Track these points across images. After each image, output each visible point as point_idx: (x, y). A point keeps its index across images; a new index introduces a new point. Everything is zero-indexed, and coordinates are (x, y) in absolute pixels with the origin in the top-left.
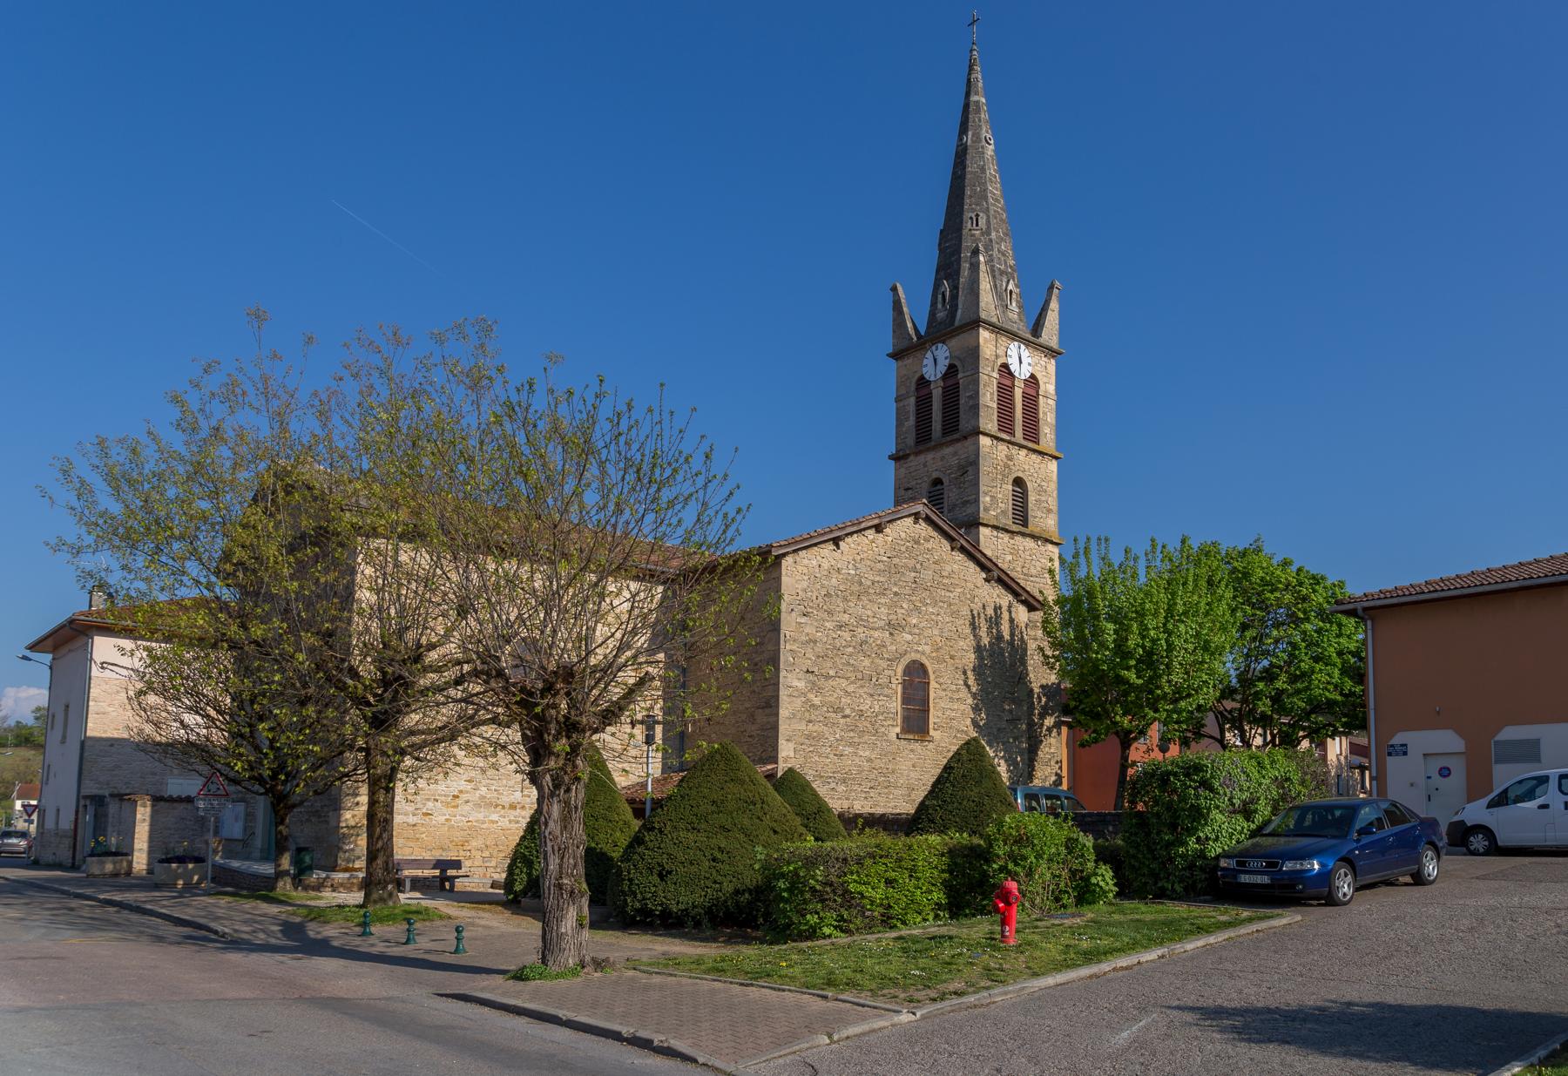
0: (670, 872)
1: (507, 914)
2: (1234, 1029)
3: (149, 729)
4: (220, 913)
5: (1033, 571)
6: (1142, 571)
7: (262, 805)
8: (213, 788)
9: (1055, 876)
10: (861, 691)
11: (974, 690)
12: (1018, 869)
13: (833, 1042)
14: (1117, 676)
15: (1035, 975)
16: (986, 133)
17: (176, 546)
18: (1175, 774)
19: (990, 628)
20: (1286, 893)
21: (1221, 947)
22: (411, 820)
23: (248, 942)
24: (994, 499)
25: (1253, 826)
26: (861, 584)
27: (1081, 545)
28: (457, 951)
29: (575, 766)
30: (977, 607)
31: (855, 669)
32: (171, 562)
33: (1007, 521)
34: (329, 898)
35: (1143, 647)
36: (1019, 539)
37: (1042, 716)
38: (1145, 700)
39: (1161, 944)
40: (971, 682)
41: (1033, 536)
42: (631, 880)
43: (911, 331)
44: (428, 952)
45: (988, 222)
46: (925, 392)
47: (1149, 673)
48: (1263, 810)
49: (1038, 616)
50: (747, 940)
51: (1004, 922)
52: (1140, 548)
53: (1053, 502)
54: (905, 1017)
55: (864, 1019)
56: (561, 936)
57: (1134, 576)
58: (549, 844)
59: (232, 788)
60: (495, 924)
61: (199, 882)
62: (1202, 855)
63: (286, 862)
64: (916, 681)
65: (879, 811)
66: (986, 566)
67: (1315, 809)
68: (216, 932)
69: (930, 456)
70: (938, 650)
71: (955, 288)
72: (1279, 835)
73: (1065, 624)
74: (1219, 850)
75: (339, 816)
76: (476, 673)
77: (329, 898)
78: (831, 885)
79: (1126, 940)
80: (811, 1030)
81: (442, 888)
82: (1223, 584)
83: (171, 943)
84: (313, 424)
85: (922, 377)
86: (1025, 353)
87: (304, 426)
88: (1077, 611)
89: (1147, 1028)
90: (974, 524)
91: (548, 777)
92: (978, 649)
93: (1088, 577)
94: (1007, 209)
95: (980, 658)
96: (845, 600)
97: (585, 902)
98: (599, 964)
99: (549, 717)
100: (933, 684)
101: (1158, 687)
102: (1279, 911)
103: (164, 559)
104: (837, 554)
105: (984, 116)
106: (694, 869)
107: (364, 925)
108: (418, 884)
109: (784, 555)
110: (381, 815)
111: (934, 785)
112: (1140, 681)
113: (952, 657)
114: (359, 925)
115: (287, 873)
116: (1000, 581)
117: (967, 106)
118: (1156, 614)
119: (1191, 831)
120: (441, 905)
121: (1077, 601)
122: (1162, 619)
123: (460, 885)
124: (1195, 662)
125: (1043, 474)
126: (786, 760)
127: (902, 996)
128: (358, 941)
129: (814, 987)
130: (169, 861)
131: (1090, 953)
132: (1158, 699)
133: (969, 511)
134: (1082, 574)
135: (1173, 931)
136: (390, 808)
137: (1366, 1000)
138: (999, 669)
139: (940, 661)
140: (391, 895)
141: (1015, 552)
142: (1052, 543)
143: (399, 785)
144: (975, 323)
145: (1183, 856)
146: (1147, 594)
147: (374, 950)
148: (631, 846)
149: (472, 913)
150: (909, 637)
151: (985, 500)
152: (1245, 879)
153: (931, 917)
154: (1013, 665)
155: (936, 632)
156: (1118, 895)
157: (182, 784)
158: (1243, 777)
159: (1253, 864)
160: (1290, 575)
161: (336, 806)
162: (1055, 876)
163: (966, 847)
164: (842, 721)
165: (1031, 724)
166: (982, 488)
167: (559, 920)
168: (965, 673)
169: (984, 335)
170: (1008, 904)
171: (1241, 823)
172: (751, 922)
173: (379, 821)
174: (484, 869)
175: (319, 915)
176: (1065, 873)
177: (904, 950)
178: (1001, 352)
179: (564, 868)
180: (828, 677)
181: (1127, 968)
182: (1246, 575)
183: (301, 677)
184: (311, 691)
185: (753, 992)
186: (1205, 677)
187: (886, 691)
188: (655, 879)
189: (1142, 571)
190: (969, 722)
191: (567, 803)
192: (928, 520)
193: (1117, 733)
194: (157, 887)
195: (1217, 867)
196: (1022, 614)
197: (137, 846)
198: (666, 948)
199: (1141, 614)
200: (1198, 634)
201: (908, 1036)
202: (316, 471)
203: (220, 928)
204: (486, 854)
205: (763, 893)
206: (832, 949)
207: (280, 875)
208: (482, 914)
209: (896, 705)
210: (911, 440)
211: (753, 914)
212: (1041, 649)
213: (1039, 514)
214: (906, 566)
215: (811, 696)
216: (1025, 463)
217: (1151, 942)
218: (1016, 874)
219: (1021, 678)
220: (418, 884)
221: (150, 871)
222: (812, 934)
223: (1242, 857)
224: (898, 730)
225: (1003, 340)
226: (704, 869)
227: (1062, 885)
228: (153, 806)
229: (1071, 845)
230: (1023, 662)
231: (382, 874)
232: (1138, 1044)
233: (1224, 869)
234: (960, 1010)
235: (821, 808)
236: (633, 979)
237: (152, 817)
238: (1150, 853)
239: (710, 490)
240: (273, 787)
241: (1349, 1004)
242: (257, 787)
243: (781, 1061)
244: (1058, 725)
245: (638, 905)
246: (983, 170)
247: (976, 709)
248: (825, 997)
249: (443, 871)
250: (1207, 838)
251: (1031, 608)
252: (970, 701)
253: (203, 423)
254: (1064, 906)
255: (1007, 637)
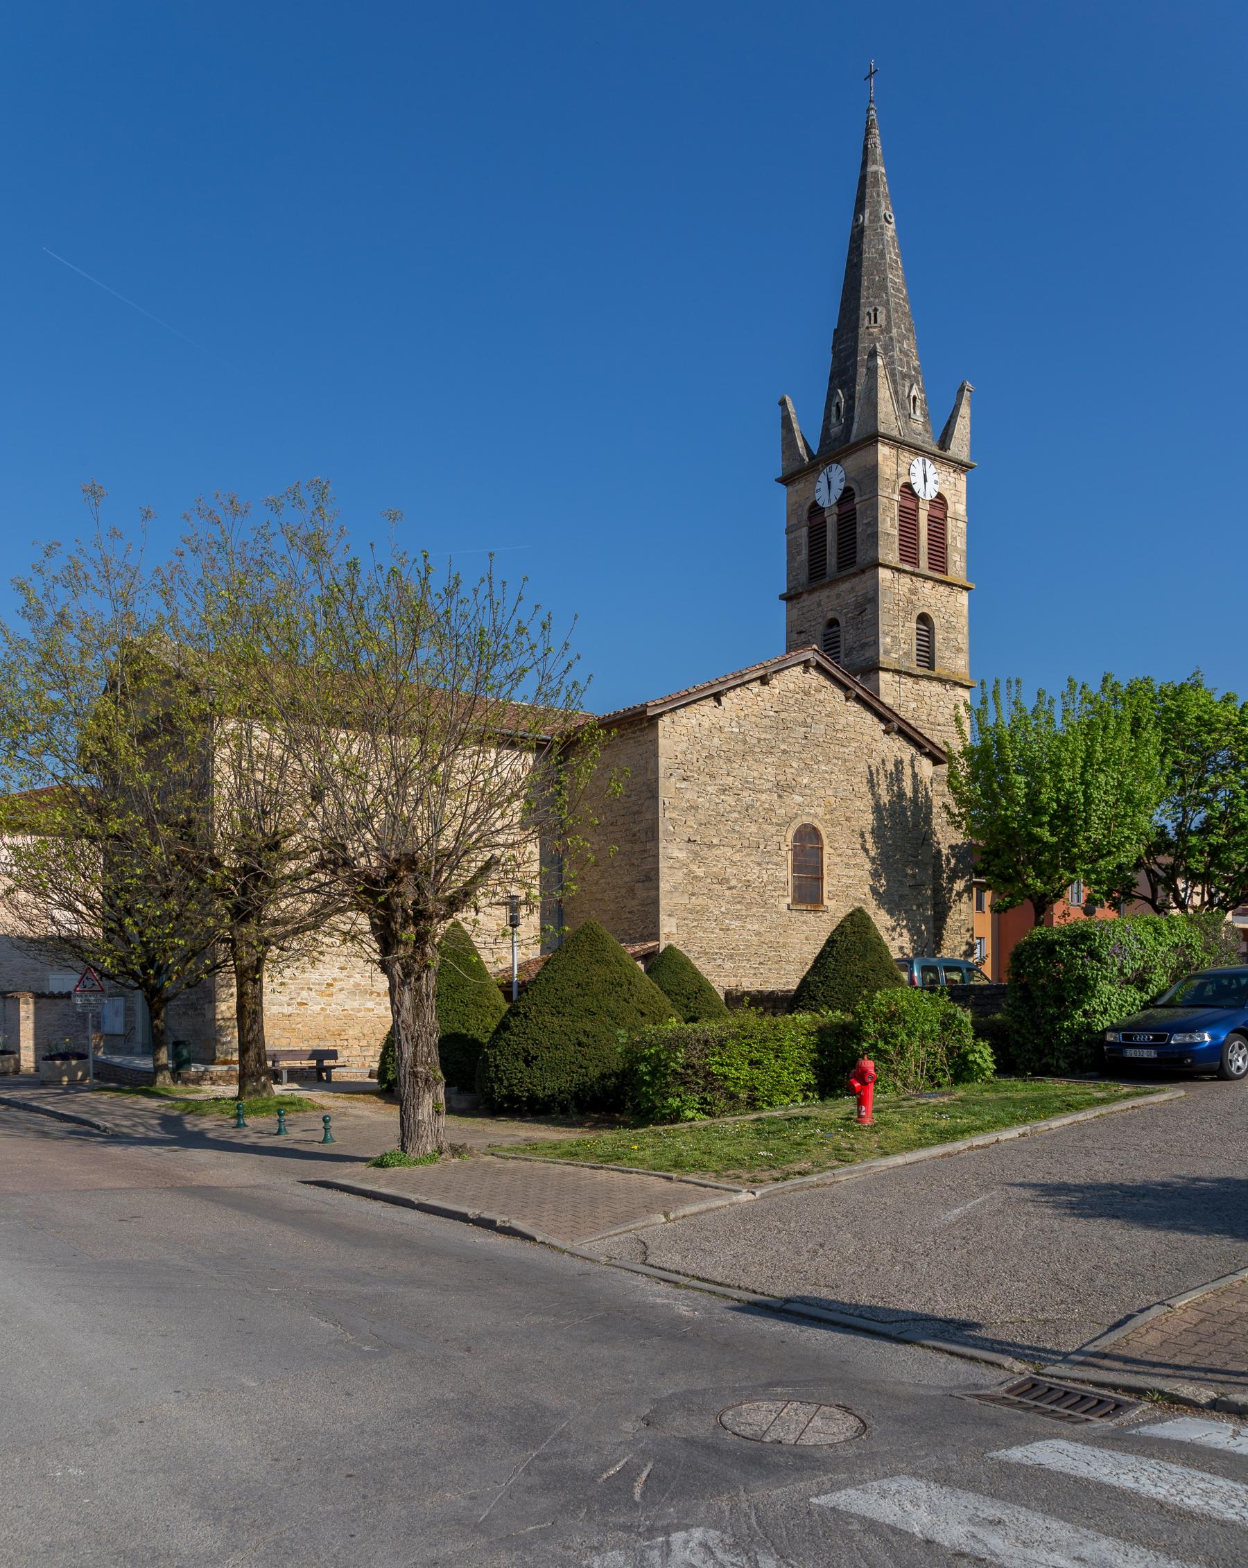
0: (535, 1058)
1: (381, 1103)
2: (1071, 1206)
3: (23, 928)
4: (102, 1108)
5: (941, 719)
6: (1057, 714)
7: (139, 996)
8: (88, 984)
9: (929, 1054)
10: (748, 860)
11: (873, 854)
12: (889, 1048)
13: (669, 1221)
14: (1030, 834)
15: (886, 1154)
16: (885, 209)
17: (31, 739)
18: (1061, 944)
19: (890, 785)
20: (1176, 1067)
21: (1090, 1124)
22: (286, 1010)
23: (128, 1136)
24: (895, 640)
25: (1146, 997)
26: (745, 742)
27: (989, 689)
28: (325, 1141)
29: (424, 954)
30: (875, 762)
31: (741, 836)
32: (27, 757)
33: (911, 665)
34: (208, 1090)
35: (1058, 801)
36: (924, 684)
37: (952, 880)
38: (1062, 859)
39: (1024, 1122)
40: (869, 845)
41: (940, 680)
42: (497, 1066)
43: (802, 451)
44: (298, 1142)
45: (888, 317)
46: (818, 520)
47: (1065, 830)
48: (1160, 979)
49: (943, 769)
50: (612, 1124)
51: (861, 1102)
52: (1055, 689)
53: (963, 640)
54: (744, 1197)
55: (703, 1198)
56: (418, 1124)
57: (1050, 721)
58: (403, 1033)
59: (106, 983)
60: (367, 1113)
61: (83, 1078)
62: (1088, 1029)
63: (164, 1056)
64: (808, 846)
65: (769, 987)
66: (885, 716)
67: (1215, 977)
68: (98, 1127)
69: (824, 594)
70: (831, 812)
71: (850, 398)
72: (1173, 1007)
73: (973, 778)
74: (1107, 1024)
75: (215, 1008)
76: (322, 865)
77: (208, 1090)
78: (693, 1067)
79: (988, 1118)
80: (649, 1209)
81: (320, 1079)
82: (1150, 726)
83: (55, 1139)
84: (157, 602)
85: (815, 504)
86: (931, 469)
87: (149, 607)
88: (987, 761)
89: (982, 1205)
90: (872, 669)
91: (398, 966)
92: (877, 809)
93: (996, 725)
94: (910, 299)
95: (879, 819)
96: (729, 760)
97: (441, 1089)
98: (456, 1150)
99: (400, 906)
100: (827, 850)
101: (1075, 845)
102: (1158, 1087)
103: (20, 753)
104: (719, 711)
105: (883, 189)
106: (559, 1054)
107: (238, 1116)
108: (295, 1075)
109: (661, 715)
110: (250, 1006)
111: (817, 960)
112: (1055, 839)
113: (848, 819)
114: (234, 1117)
115: (165, 1067)
116: (901, 732)
117: (863, 178)
118: (1072, 765)
119: (1077, 1004)
120: (318, 1096)
121: (984, 752)
122: (1078, 770)
123: (337, 1075)
124: (1116, 816)
125: (952, 608)
126: (668, 937)
127: (746, 1176)
128: (232, 1133)
129: (660, 1169)
130: (52, 1058)
131: (947, 1132)
132: (1074, 859)
133: (867, 655)
134: (990, 722)
135: (1042, 1108)
136: (258, 998)
137: (1216, 1175)
138: (900, 835)
139: (834, 823)
140: (264, 1086)
141: (919, 698)
142: (962, 686)
143: (266, 975)
144: (873, 438)
145: (1068, 1030)
146: (1063, 741)
147: (246, 1141)
148: (497, 1032)
149: (346, 1103)
150: (799, 799)
151: (885, 641)
152: (1131, 1053)
153: (799, 1099)
154: (916, 825)
155: (830, 792)
156: (996, 1073)
157: (63, 981)
158: (1136, 945)
159: (1141, 1038)
160: (1230, 714)
161: (211, 998)
162: (929, 1054)
163: (837, 1025)
164: (728, 893)
165: (937, 890)
166: (882, 628)
167: (416, 1107)
168: (862, 835)
169: (883, 451)
170: (864, 1083)
171: (1134, 996)
172: (619, 1107)
173: (249, 1013)
174: (359, 1060)
175: (196, 1108)
176: (941, 1052)
177: (758, 1132)
178: (903, 470)
179: (425, 1058)
180: (711, 846)
181: (983, 1147)
182: (1180, 716)
183: (162, 871)
184: (171, 884)
185: (602, 1175)
186: (1127, 833)
187: (775, 859)
188: (522, 1065)
189: (1057, 714)
190: (867, 889)
191: (418, 991)
192: (819, 667)
193: (1030, 897)
194: (43, 1084)
195: (1103, 1041)
196: (926, 768)
197: (23, 1044)
198: (530, 1134)
199: (1056, 764)
200: (1120, 784)
201: (746, 1215)
202: (166, 651)
203: (101, 1123)
204: (364, 1043)
205: (627, 1077)
206: (693, 1131)
207: (159, 1069)
208: (355, 1104)
209: (786, 873)
210: (803, 576)
211: (618, 1099)
212: (946, 807)
213: (947, 654)
214: (794, 721)
215: (694, 867)
216: (931, 597)
217: (1015, 1120)
218: (886, 1052)
219: (924, 837)
220: (295, 1075)
221: (37, 1069)
222: (676, 1117)
223: (1128, 1030)
224: (789, 900)
225: (905, 456)
226: (576, 1055)
227: (938, 1063)
228: (35, 1003)
229: (947, 1022)
230: (928, 820)
231: (256, 1067)
232: (967, 1219)
233: (1110, 1043)
234: (802, 1189)
235: (702, 988)
236: (488, 1164)
237: (36, 1014)
238: (1034, 1027)
239: (549, 663)
240: (146, 981)
241: (1198, 1179)
242: (131, 982)
243: (616, 1239)
244: (968, 889)
245: (505, 1091)
246: (882, 254)
247: (875, 875)
248: (670, 1179)
249: (320, 1061)
250: (1095, 1011)
251: (936, 761)
252: (868, 866)
253: (48, 609)
254: (939, 1085)
255: (909, 794)
